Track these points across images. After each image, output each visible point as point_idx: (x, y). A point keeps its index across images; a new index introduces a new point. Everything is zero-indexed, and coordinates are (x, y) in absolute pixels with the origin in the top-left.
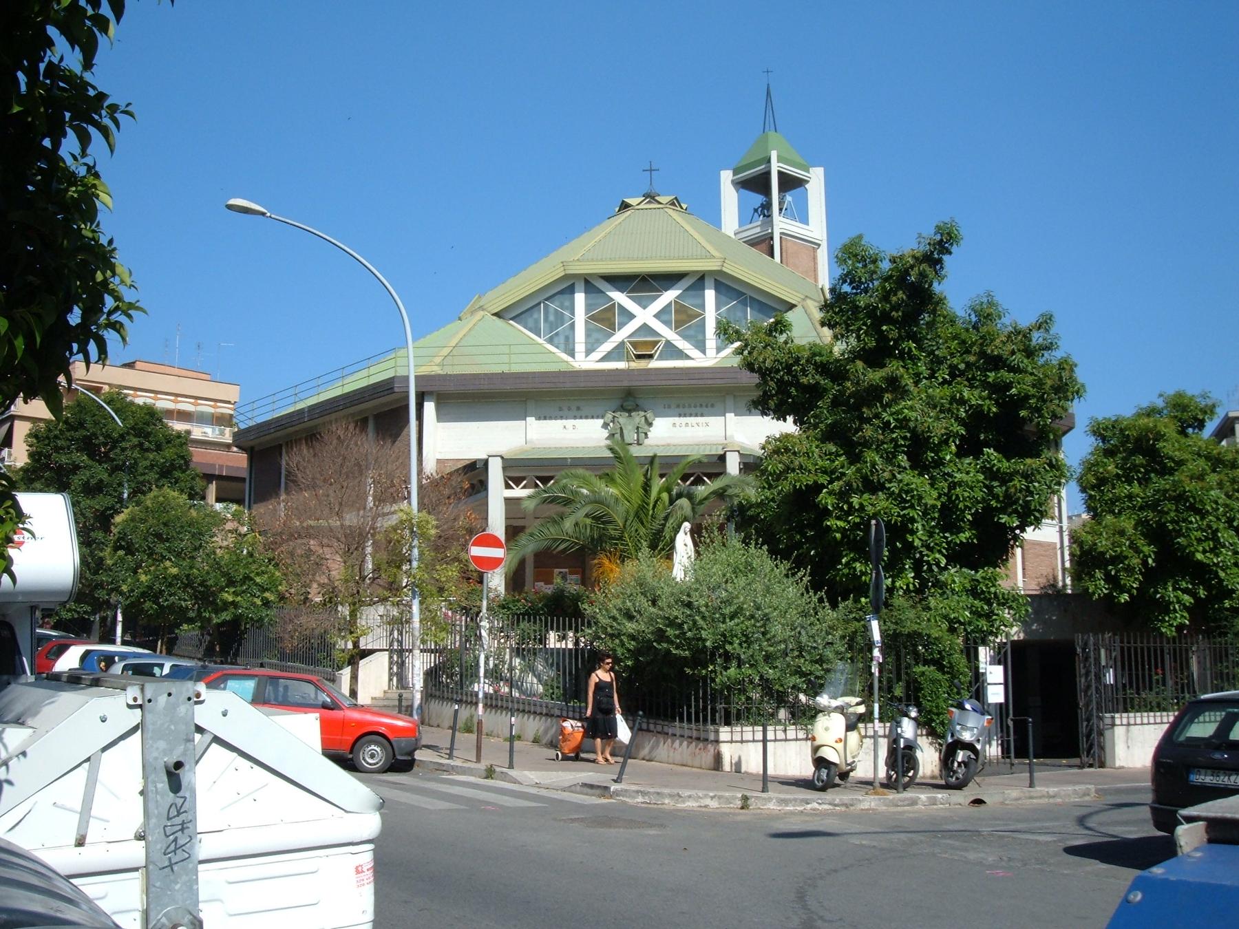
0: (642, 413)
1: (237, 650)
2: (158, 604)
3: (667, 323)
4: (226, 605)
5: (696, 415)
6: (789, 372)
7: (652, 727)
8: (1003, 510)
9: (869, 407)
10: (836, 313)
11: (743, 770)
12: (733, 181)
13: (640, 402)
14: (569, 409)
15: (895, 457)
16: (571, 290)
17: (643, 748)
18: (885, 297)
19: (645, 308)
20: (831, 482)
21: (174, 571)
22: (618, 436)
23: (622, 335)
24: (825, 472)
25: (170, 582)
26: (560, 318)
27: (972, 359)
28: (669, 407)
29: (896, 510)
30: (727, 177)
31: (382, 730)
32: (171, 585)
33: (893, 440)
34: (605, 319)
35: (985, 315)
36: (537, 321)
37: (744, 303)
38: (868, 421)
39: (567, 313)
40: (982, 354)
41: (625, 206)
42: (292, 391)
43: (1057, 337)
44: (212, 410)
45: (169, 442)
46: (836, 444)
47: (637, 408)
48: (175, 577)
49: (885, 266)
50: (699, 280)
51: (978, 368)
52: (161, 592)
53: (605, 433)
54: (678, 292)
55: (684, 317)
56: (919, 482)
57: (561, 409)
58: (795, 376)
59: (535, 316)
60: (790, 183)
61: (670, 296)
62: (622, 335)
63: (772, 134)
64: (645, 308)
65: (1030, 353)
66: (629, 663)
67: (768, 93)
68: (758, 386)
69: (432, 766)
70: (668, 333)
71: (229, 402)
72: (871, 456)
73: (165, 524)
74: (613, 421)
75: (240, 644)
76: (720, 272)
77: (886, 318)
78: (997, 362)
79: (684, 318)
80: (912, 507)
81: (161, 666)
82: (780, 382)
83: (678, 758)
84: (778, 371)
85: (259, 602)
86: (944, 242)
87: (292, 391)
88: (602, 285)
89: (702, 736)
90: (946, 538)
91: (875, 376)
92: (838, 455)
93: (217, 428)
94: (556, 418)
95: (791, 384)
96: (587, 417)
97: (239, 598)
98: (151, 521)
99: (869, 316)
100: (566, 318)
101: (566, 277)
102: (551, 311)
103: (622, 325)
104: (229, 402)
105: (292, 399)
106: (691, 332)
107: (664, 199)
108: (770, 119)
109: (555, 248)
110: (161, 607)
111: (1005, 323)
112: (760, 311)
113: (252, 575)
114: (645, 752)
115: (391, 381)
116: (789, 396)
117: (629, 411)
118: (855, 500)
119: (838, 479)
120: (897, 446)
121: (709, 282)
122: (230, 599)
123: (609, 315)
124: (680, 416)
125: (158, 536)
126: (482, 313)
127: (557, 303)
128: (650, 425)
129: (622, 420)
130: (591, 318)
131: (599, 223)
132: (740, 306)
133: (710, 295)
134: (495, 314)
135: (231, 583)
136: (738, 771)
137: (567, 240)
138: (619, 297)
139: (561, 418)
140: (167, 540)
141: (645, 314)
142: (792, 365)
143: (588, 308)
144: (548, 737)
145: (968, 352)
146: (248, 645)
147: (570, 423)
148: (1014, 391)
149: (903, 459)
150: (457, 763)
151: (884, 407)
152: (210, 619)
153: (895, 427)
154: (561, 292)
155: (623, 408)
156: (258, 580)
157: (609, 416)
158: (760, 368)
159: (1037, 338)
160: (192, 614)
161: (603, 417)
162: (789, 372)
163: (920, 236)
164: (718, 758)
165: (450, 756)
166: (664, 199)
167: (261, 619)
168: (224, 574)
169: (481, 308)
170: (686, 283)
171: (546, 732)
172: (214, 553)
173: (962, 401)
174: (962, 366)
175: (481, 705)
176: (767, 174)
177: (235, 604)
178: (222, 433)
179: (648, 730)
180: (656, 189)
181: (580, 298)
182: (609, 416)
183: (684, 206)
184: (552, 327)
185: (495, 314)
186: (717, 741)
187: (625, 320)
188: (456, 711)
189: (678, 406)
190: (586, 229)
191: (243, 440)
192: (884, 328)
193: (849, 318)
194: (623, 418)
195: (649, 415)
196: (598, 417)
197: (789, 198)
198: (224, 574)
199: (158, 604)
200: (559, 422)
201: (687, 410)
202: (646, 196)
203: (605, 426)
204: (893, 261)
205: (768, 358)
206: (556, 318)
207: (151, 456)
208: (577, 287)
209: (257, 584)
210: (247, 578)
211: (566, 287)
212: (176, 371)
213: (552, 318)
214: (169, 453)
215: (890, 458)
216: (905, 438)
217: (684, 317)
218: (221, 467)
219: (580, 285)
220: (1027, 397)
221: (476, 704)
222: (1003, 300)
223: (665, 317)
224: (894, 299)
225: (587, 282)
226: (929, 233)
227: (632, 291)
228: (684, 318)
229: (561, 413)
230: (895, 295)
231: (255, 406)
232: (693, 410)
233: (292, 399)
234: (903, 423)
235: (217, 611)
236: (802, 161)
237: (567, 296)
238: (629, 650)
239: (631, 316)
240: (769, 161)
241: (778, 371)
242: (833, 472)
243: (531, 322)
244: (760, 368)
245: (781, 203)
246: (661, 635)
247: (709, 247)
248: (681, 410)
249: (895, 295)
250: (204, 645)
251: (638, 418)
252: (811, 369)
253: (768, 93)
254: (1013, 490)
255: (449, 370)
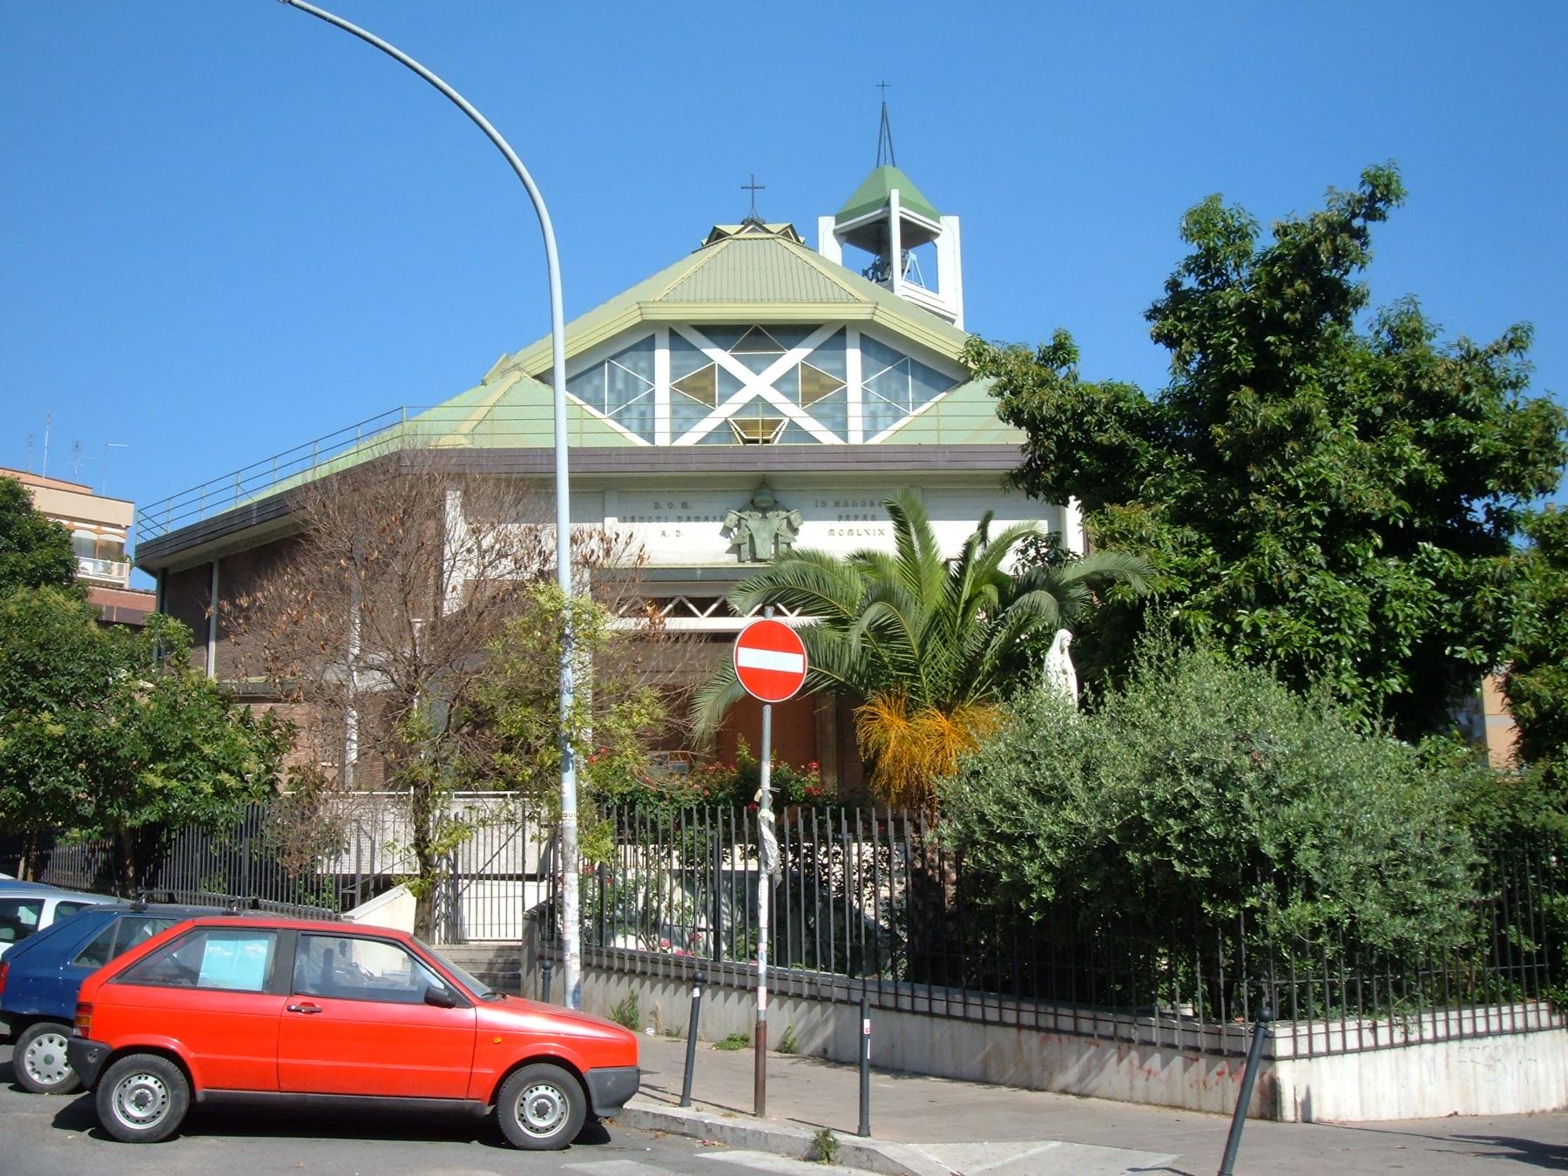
0: (783, 514)
1: (154, 875)
2: (27, 790)
3: (791, 396)
4: (150, 794)
5: (865, 518)
6: (1078, 425)
7: (1086, 1026)
8: (1458, 639)
9: (1260, 464)
10: (1179, 319)
11: (1315, 1115)
12: (835, 232)
13: (780, 497)
14: (671, 506)
15: (1303, 546)
16: (649, 345)
17: (1063, 1068)
18: (1274, 289)
19: (758, 373)
20: (1194, 590)
21: (58, 730)
22: (745, 548)
23: (725, 411)
24: (1181, 574)
25: (48, 749)
26: (632, 385)
27: (1395, 397)
28: (824, 505)
29: (1313, 633)
30: (827, 225)
31: (553, 1049)
32: (50, 755)
33: (1301, 517)
34: (700, 389)
35: (1406, 334)
36: (598, 390)
37: (903, 369)
38: (1259, 487)
39: (643, 378)
40: (1412, 391)
41: (717, 236)
42: (231, 480)
43: (1529, 366)
44: (94, 537)
45: (41, 539)
46: (1195, 528)
47: (775, 506)
48: (57, 740)
49: (1264, 242)
50: (839, 334)
51: (1405, 414)
52: (33, 769)
53: (727, 544)
54: (808, 351)
55: (816, 388)
56: (1339, 586)
57: (657, 506)
58: (1087, 432)
59: (596, 381)
60: (916, 236)
61: (795, 356)
62: (725, 411)
63: (889, 168)
64: (758, 373)
65: (1494, 386)
66: (1049, 894)
67: (884, 115)
68: (1024, 449)
69: (648, 1123)
70: (792, 411)
71: (119, 526)
72: (1269, 543)
73: (42, 647)
74: (738, 526)
75: (158, 866)
76: (870, 323)
77: (1276, 324)
78: (1437, 404)
79: (817, 389)
80: (1340, 630)
81: (37, 906)
82: (1063, 441)
83: (1158, 1090)
84: (1057, 424)
85: (208, 789)
86: (1378, 196)
87: (231, 480)
88: (696, 338)
89: (1226, 1044)
90: (1369, 685)
91: (1272, 412)
92: (1201, 546)
93: (100, 562)
94: (650, 520)
95: (1078, 445)
96: (697, 519)
97: (174, 783)
98: (16, 642)
99: (1242, 321)
100: (642, 386)
101: (644, 325)
102: (620, 375)
103: (724, 398)
104: (119, 526)
105: (232, 493)
106: (826, 410)
107: (775, 228)
108: (886, 149)
109: (636, 281)
110: (33, 796)
111: (1443, 345)
112: (926, 381)
113: (197, 741)
114: (1070, 1076)
115: (398, 457)
116: (1077, 463)
117: (764, 510)
118: (1244, 618)
119: (1205, 585)
120: (1310, 527)
121: (852, 338)
122: (158, 783)
123: (705, 383)
124: (840, 518)
125: (29, 668)
126: (516, 375)
127: (628, 363)
128: (795, 531)
129: (751, 523)
130: (680, 386)
131: (680, 258)
132: (896, 373)
133: (854, 356)
134: (536, 377)
135: (159, 754)
136: (1307, 1120)
137: (648, 274)
138: (720, 356)
139: (659, 519)
140: (46, 674)
141: (759, 381)
142: (1083, 414)
143: (675, 371)
144: (817, 1042)
145: (1386, 388)
146: (173, 867)
147: (671, 527)
148: (1475, 448)
149: (1314, 550)
150: (712, 1117)
151: (1287, 464)
152: (118, 821)
153: (1308, 497)
154: (635, 348)
155: (753, 505)
156: (207, 749)
157: (732, 517)
158: (1032, 415)
159: (1506, 365)
160: (89, 810)
161: (722, 519)
162: (1078, 425)
163: (1331, 190)
164: (1272, 1093)
165: (685, 1100)
166: (775, 228)
167: (212, 821)
168: (150, 738)
169: (517, 367)
170: (818, 338)
171: (811, 1032)
172: (132, 700)
173: (1397, 462)
174: (1379, 411)
175: (762, 991)
176: (882, 225)
177: (167, 796)
178: (108, 570)
179: (1077, 1033)
180: (760, 215)
181: (662, 356)
182: (732, 517)
183: (802, 239)
184: (621, 398)
185: (536, 377)
186: (1271, 1059)
187: (728, 390)
188: (696, 1003)
189: (837, 504)
190: (665, 265)
191: (149, 557)
192: (1270, 338)
193: (1203, 326)
194: (753, 521)
195: (794, 516)
196: (714, 519)
197: (912, 256)
198: (150, 738)
199: (27, 790)
200: (655, 524)
201: (853, 511)
202: (746, 223)
203: (726, 531)
204: (1282, 232)
205: (1047, 403)
206: (626, 384)
207: (12, 559)
208: (658, 340)
209: (204, 758)
210: (188, 746)
211: (643, 338)
212: (44, 482)
213: (620, 385)
214: (42, 555)
215: (1296, 550)
216: (1320, 515)
217: (816, 388)
218: (110, 609)
219: (663, 339)
220: (1499, 458)
221: (755, 990)
222: (1430, 314)
223: (788, 388)
224: (1289, 291)
225: (673, 334)
226: (1354, 188)
227: (735, 350)
228: (817, 389)
229: (658, 512)
230: (1291, 285)
231: (204, 492)
232: (859, 510)
233: (232, 493)
234: (1320, 490)
235: (134, 805)
236: (926, 204)
237: (644, 354)
238: (1048, 868)
239: (739, 385)
240: (888, 204)
241: (1057, 424)
242: (1195, 574)
243: (588, 391)
244: (1032, 415)
245: (904, 262)
246: (1135, 831)
247: (850, 289)
248: (842, 510)
249: (1291, 285)
250: (95, 869)
251: (777, 520)
252: (1112, 420)
253: (884, 115)
254: (1479, 607)
255: (485, 443)
